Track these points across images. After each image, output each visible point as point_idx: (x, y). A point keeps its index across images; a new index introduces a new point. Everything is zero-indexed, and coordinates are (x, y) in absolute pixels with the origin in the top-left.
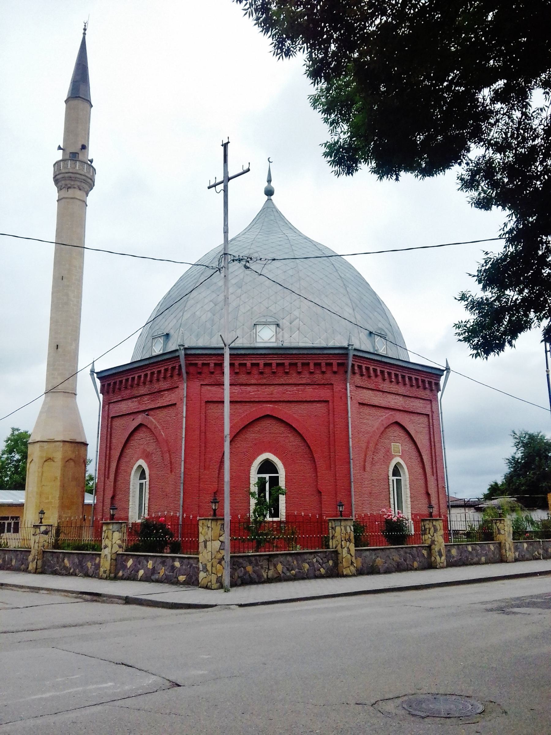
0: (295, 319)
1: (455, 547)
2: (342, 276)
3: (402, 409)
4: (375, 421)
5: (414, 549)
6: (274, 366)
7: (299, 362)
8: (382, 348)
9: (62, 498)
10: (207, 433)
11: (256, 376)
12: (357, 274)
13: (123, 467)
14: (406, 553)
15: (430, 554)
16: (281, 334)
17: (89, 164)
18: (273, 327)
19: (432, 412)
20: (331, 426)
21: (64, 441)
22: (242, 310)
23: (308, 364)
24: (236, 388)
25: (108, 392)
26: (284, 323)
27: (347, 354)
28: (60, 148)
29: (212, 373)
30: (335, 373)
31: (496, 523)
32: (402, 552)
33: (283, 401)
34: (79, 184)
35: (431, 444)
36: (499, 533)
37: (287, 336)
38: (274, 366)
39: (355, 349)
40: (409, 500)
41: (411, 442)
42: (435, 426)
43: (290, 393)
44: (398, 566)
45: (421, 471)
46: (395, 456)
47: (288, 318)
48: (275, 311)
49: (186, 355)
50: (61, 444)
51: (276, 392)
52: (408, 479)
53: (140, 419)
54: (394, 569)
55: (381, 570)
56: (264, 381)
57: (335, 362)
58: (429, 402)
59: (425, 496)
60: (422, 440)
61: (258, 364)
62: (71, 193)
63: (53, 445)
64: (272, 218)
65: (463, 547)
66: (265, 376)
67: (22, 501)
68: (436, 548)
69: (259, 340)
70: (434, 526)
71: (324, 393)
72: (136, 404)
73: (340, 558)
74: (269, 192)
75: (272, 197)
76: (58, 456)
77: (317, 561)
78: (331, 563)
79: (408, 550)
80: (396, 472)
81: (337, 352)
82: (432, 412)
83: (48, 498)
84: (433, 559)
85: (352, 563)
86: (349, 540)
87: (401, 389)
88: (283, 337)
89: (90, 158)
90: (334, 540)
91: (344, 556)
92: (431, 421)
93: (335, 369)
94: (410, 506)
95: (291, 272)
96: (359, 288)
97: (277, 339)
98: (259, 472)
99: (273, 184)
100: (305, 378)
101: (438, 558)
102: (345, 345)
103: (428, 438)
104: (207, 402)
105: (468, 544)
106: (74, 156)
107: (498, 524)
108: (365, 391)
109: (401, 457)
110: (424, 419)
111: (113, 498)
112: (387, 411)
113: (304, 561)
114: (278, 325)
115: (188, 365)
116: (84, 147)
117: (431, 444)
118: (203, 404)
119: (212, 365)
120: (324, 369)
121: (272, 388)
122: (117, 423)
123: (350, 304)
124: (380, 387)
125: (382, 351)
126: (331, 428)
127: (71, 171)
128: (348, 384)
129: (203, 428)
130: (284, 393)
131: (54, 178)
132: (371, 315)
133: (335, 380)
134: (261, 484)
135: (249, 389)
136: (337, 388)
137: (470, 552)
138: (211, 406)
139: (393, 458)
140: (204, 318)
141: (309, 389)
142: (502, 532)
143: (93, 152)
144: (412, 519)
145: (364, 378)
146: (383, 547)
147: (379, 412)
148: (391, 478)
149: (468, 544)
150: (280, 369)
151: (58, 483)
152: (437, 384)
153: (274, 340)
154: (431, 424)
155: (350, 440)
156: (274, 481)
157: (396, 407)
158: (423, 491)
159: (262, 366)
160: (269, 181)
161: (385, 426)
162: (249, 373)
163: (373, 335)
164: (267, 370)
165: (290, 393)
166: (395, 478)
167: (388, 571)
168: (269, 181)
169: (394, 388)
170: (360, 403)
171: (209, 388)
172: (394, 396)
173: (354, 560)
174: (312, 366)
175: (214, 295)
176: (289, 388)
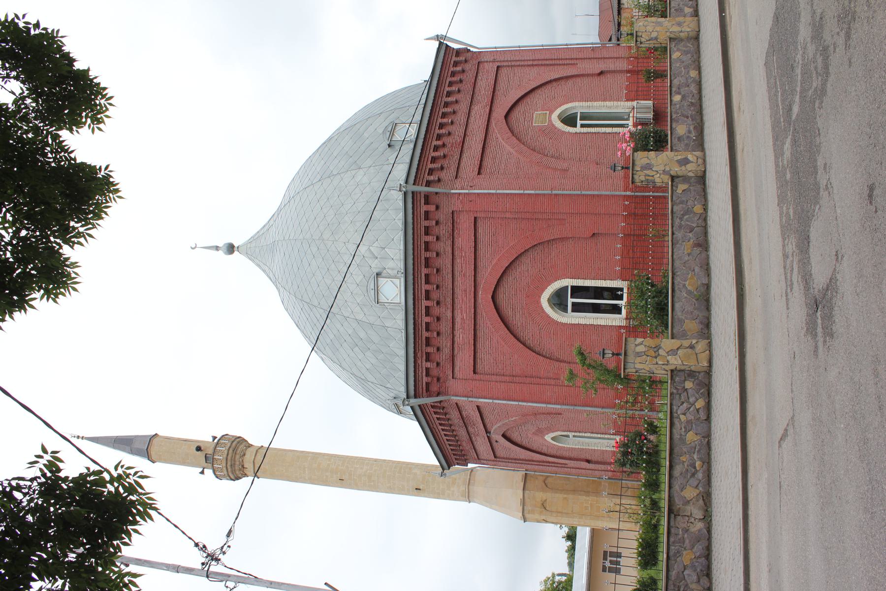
0: (370, 250)
1: (674, 126)
2: (319, 177)
3: (488, 107)
4: (503, 144)
5: (675, 208)
6: (428, 287)
7: (424, 255)
8: (408, 132)
9: (587, 493)
10: (514, 373)
11: (443, 310)
12: (318, 154)
13: (554, 452)
14: (680, 227)
15: (685, 179)
16: (390, 271)
17: (218, 442)
18: (382, 281)
19: (494, 61)
20: (508, 215)
21: (524, 489)
22: (360, 316)
23: (427, 243)
24: (457, 335)
25: (466, 460)
26: (376, 266)
27: (413, 193)
28: (202, 472)
29: (438, 364)
30: (437, 208)
31: (641, 43)
32: (679, 235)
33: (475, 276)
34: (238, 457)
35: (536, 65)
36: (656, 39)
37: (391, 264)
38: (428, 287)
39: (406, 182)
40: (608, 103)
41: (532, 95)
42: (512, 58)
43: (464, 266)
44: (699, 245)
45: (570, 82)
46: (550, 120)
47: (370, 262)
48: (362, 277)
49: (415, 397)
50: (527, 492)
51: (464, 284)
52: (581, 104)
53: (496, 437)
54: (703, 255)
55: (705, 281)
56: (449, 300)
57: (424, 208)
58: (481, 66)
59: (602, 77)
60: (533, 77)
61: (427, 308)
62: (248, 465)
63: (527, 500)
64: (257, 250)
65: (676, 113)
66: (442, 299)
67: (588, 529)
68: (676, 170)
69: (397, 300)
70: (644, 168)
71: (465, 224)
72: (478, 438)
73: (683, 368)
74: (231, 249)
75: (236, 245)
76: (540, 495)
77: (684, 414)
78: (689, 385)
79: (677, 221)
80: (570, 120)
81: (410, 206)
82: (494, 61)
83: (586, 508)
84: (691, 174)
85: (692, 347)
86: (658, 348)
87: (463, 108)
88: (393, 269)
89: (211, 440)
90: (655, 372)
91: (680, 362)
92: (506, 64)
93: (432, 208)
94: (615, 103)
95: (314, 249)
96: (335, 154)
97: (395, 277)
98: (565, 310)
99: (220, 245)
100: (444, 246)
101: (690, 167)
102: (400, 196)
103: (527, 69)
104: (475, 372)
105: (671, 101)
106: (210, 460)
107: (643, 40)
108: (462, 164)
109: (551, 112)
110: (503, 72)
111: (588, 461)
112: (490, 130)
113: (682, 440)
114: (378, 275)
115: (429, 392)
116: (199, 449)
117: (536, 65)
118: (476, 376)
119: (428, 365)
120: (434, 223)
121: (458, 291)
122: (500, 452)
123: (354, 172)
124: (459, 140)
125: (413, 131)
126: (511, 216)
127: (224, 465)
128: (453, 191)
129: (507, 379)
130: (464, 275)
131: (232, 480)
132: (368, 142)
133: (447, 208)
134: (577, 308)
135: (458, 320)
136: (456, 205)
137: (684, 97)
138: (479, 367)
139: (553, 125)
140: (374, 361)
141: (459, 242)
142: (654, 35)
143: (205, 436)
144: (632, 100)
145: (445, 166)
146: (670, 274)
147: (491, 143)
148: (578, 129)
149: (671, 101)
150: (432, 279)
151: (571, 496)
152: (458, 52)
153: (397, 281)
154: (510, 64)
155: (526, 192)
156: (577, 291)
157: (486, 117)
158: (597, 79)
159: (428, 303)
160: (217, 248)
161: (510, 134)
162: (438, 319)
163: (392, 143)
164: (434, 295)
165: (464, 266)
166: (579, 122)
167: (707, 269)
168: (217, 248)
169: (461, 118)
170: (479, 173)
171: (457, 369)
172: (472, 119)
173: (686, 343)
174: (429, 238)
175: (345, 345)
176: (457, 268)
